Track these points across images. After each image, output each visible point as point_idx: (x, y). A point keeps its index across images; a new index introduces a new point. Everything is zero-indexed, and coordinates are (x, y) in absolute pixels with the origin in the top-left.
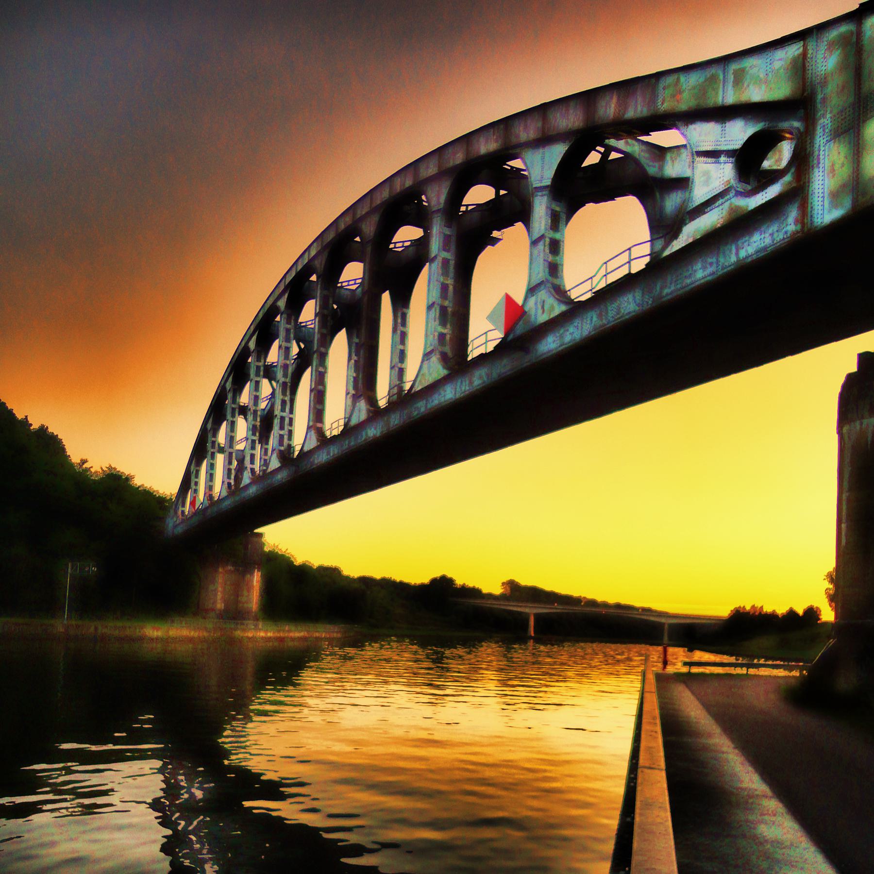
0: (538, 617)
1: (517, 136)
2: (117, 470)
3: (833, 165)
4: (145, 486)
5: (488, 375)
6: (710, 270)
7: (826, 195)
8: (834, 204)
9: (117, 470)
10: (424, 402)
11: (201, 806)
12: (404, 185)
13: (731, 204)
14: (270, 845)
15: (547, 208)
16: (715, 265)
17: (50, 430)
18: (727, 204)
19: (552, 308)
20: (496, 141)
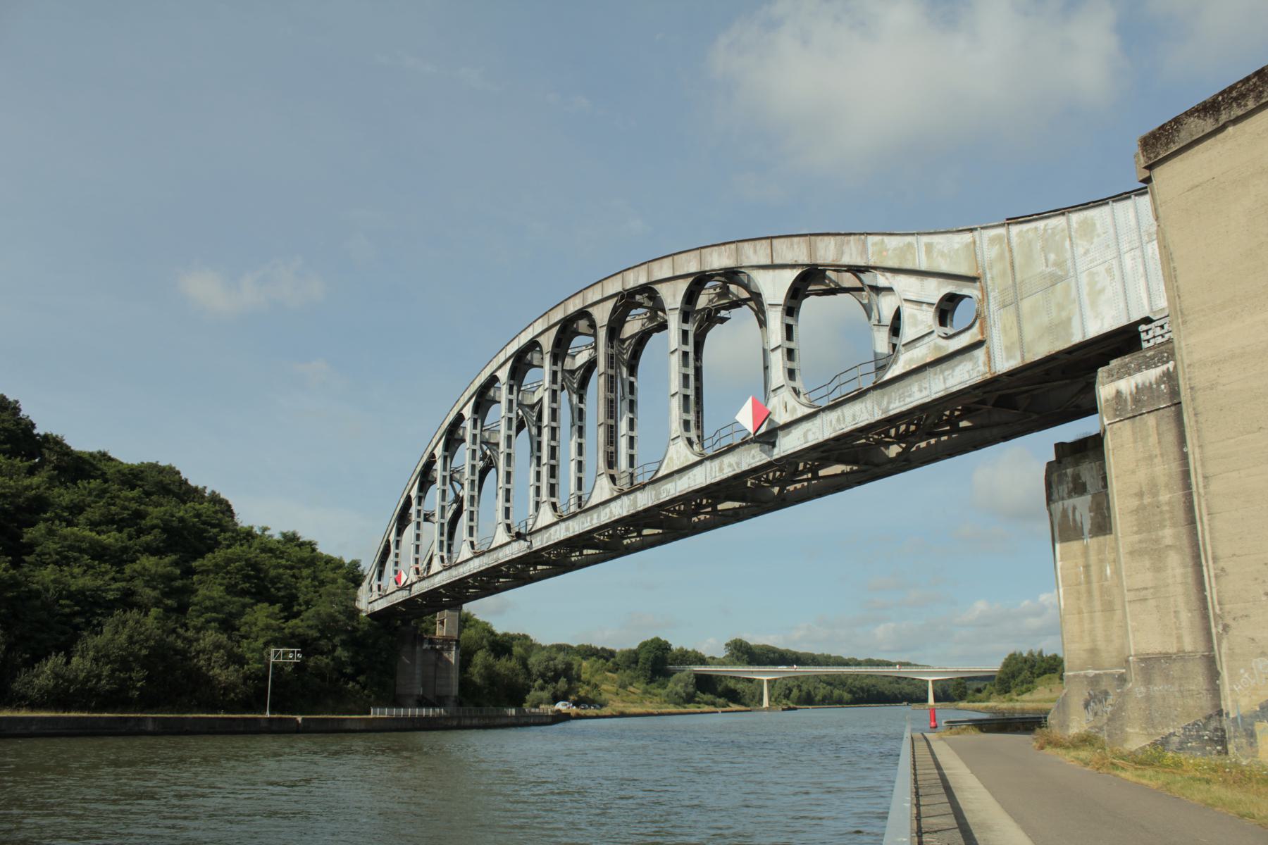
0: (934, 682)
1: (748, 258)
2: (301, 540)
3: (1005, 326)
4: (317, 547)
5: (738, 464)
6: (925, 393)
7: (1003, 348)
8: (1009, 357)
9: (301, 540)
10: (674, 484)
11: (944, 441)
12: (638, 280)
13: (935, 343)
14: (774, 496)
15: (782, 323)
16: (928, 390)
17: (145, 462)
18: (932, 343)
19: (794, 409)
20: (729, 257)
